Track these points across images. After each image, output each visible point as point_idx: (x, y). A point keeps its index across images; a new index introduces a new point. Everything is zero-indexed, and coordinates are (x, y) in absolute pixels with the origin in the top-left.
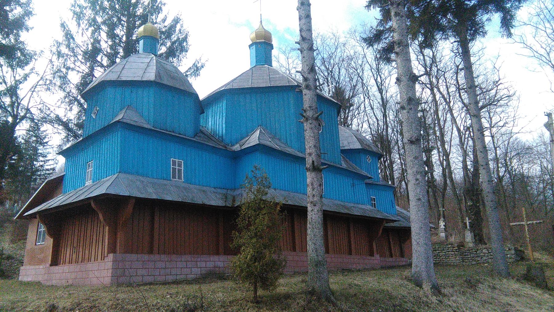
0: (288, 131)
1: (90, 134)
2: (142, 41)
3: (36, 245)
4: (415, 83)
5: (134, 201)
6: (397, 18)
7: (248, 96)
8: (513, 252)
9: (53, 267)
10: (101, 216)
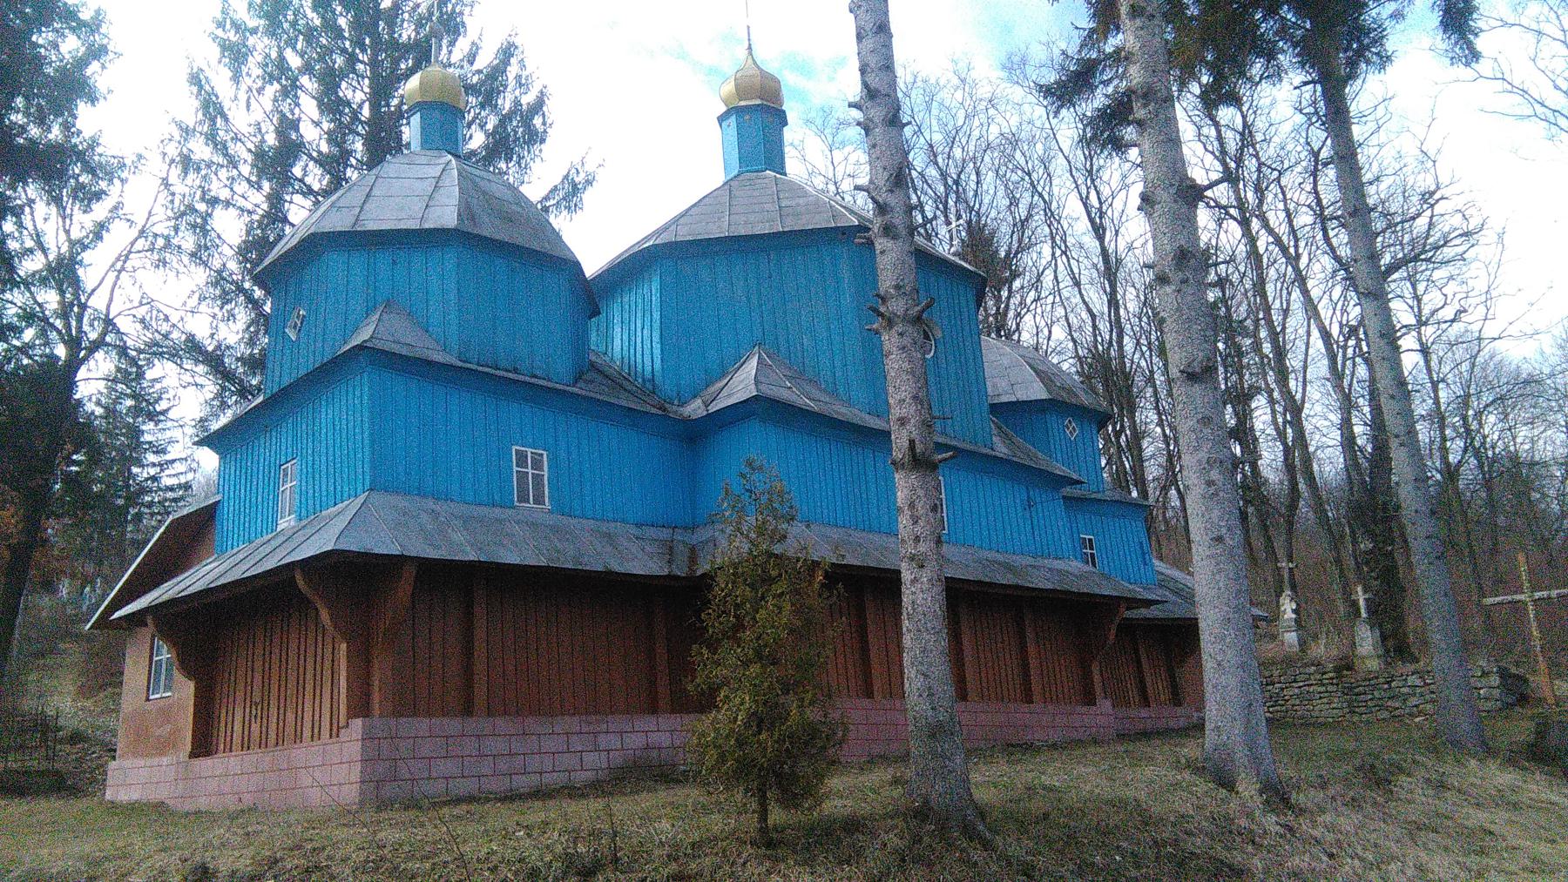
5: (410, 572)
6: (1138, 22)
8: (1495, 680)
9: (197, 762)
10: (325, 615)
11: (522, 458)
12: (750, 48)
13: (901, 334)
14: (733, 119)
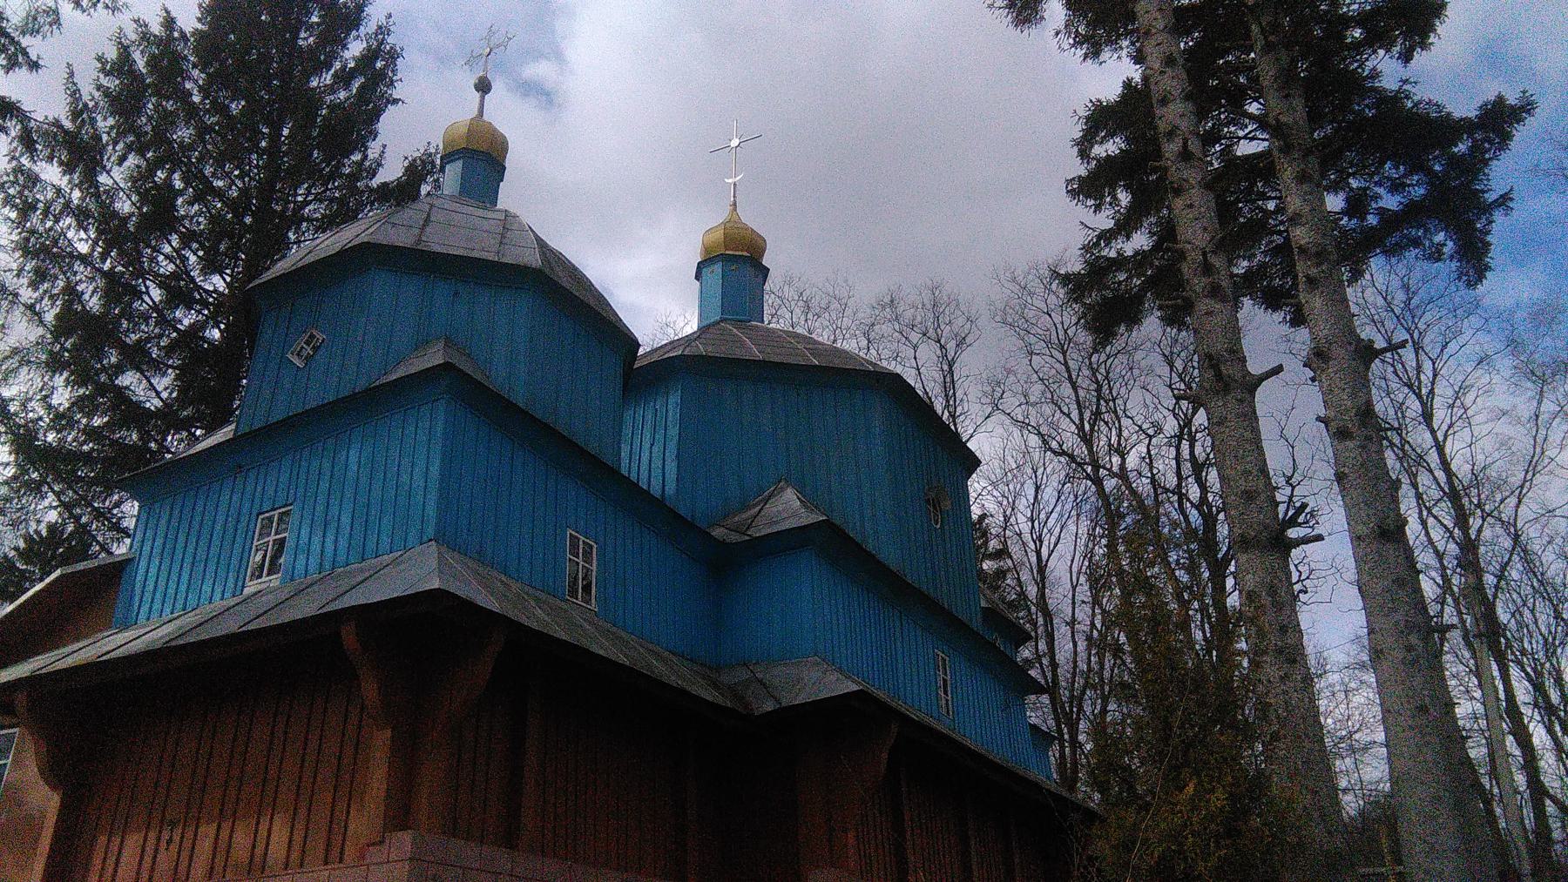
1: (272, 420)
2: (459, 164)
6: (1305, 187)
10: (370, 689)
13: (1241, 401)
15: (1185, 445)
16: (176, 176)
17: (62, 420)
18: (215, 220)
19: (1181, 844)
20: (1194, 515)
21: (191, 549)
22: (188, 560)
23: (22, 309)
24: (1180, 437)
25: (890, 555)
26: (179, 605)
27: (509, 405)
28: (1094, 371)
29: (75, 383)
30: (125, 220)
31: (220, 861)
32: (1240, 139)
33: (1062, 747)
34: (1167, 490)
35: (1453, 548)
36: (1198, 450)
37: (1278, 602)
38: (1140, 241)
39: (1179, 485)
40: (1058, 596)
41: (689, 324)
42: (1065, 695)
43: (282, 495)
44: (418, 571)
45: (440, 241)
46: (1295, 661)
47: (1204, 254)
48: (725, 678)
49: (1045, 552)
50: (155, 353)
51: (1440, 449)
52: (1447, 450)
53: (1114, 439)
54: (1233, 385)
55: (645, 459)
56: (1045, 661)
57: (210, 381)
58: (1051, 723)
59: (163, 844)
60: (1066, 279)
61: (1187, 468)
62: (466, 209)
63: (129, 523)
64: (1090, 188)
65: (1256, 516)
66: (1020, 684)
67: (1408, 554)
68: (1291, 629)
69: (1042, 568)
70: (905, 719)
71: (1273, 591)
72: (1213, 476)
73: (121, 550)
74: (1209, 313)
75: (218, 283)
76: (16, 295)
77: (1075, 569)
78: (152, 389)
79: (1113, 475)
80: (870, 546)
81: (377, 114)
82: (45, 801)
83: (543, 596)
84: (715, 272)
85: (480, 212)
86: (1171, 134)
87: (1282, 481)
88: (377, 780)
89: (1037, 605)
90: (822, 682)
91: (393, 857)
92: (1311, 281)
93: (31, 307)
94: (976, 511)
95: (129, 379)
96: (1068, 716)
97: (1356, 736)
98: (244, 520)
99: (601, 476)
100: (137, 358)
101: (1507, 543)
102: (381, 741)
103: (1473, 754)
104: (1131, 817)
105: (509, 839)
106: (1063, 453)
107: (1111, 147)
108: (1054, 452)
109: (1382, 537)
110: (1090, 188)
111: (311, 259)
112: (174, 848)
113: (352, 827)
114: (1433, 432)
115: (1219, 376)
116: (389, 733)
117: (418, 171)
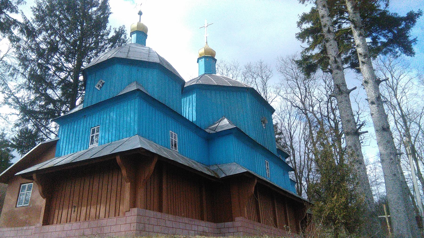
0: (246, 123)
3: (16, 207)
4: (378, 85)
5: (156, 160)
6: (361, 37)
7: (213, 92)
9: (45, 227)
10: (124, 172)
11: (172, 134)
12: (207, 42)
14: (203, 59)
15: (329, 104)
16: (57, 37)
17: (33, 103)
18: (68, 48)
19: (333, 211)
20: (332, 123)
21: (74, 137)
22: (74, 140)
23: (20, 74)
24: (328, 102)
25: (253, 135)
26: (72, 151)
27: (154, 99)
28: (305, 84)
29: (35, 93)
30: (44, 50)
31: (88, 216)
32: (343, 23)
33: (298, 184)
34: (325, 116)
35: (403, 131)
36: (333, 105)
37: (356, 149)
38: (316, 51)
39: (328, 115)
40: (296, 146)
41: (196, 75)
42: (298, 171)
43: (97, 123)
44: (134, 143)
45: (133, 56)
46: (361, 164)
47: (335, 58)
48: (212, 168)
49: (292, 132)
50: (55, 85)
51: (399, 104)
52: (401, 104)
53: (310, 103)
54: (344, 92)
55: (187, 112)
56: (293, 162)
57: (70, 90)
58: (295, 178)
59: (73, 212)
60: (297, 62)
61: (330, 110)
62: (138, 47)
63: (53, 130)
64: (302, 36)
65: (350, 126)
66: (287, 168)
67: (391, 134)
68: (360, 155)
69: (291, 138)
70: (259, 179)
71: (355, 146)
72: (337, 112)
73: (53, 137)
74: (337, 73)
75: (70, 66)
76: (19, 71)
77: (300, 138)
78: (56, 94)
79: (310, 112)
80: (247, 134)
81: (108, 17)
82: (42, 202)
83: (166, 149)
84: (202, 61)
85: (142, 48)
86: (325, 26)
87: (355, 113)
88: (127, 195)
89: (290, 147)
90: (236, 169)
91: (132, 214)
92: (363, 62)
93: (22, 74)
94: (274, 122)
95: (50, 92)
96: (299, 177)
97: (377, 181)
98: (87, 130)
99: (177, 116)
100: (51, 86)
101: (418, 128)
102: (127, 186)
103: (408, 185)
104: (321, 203)
105: (160, 210)
106: (297, 106)
107: (307, 25)
108: (294, 106)
109: (384, 129)
110: (302, 36)
111: (99, 62)
112: (76, 213)
113: (120, 208)
114: (397, 99)
115: (340, 90)
116: (129, 184)
117: (120, 33)
